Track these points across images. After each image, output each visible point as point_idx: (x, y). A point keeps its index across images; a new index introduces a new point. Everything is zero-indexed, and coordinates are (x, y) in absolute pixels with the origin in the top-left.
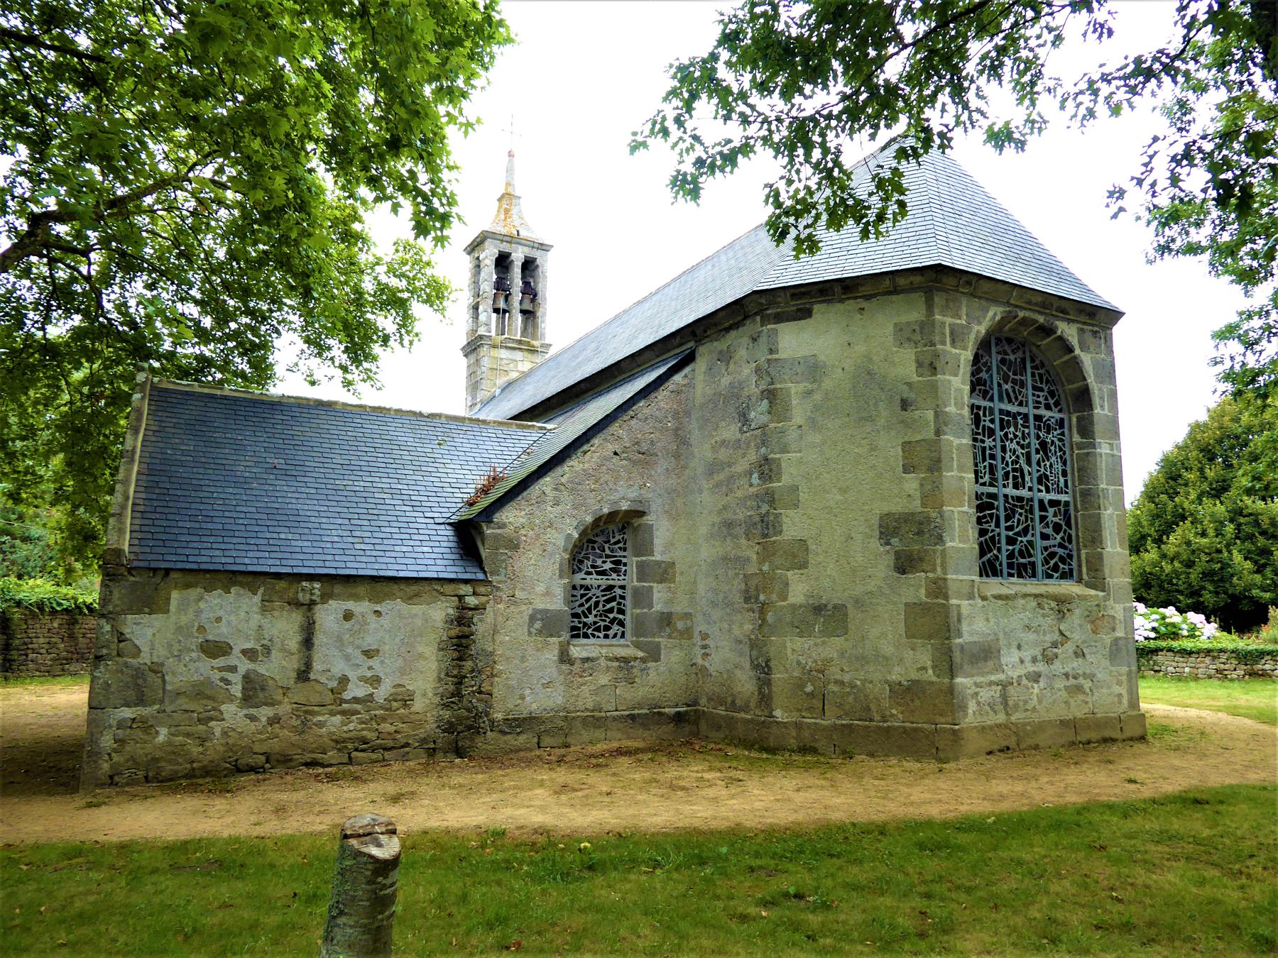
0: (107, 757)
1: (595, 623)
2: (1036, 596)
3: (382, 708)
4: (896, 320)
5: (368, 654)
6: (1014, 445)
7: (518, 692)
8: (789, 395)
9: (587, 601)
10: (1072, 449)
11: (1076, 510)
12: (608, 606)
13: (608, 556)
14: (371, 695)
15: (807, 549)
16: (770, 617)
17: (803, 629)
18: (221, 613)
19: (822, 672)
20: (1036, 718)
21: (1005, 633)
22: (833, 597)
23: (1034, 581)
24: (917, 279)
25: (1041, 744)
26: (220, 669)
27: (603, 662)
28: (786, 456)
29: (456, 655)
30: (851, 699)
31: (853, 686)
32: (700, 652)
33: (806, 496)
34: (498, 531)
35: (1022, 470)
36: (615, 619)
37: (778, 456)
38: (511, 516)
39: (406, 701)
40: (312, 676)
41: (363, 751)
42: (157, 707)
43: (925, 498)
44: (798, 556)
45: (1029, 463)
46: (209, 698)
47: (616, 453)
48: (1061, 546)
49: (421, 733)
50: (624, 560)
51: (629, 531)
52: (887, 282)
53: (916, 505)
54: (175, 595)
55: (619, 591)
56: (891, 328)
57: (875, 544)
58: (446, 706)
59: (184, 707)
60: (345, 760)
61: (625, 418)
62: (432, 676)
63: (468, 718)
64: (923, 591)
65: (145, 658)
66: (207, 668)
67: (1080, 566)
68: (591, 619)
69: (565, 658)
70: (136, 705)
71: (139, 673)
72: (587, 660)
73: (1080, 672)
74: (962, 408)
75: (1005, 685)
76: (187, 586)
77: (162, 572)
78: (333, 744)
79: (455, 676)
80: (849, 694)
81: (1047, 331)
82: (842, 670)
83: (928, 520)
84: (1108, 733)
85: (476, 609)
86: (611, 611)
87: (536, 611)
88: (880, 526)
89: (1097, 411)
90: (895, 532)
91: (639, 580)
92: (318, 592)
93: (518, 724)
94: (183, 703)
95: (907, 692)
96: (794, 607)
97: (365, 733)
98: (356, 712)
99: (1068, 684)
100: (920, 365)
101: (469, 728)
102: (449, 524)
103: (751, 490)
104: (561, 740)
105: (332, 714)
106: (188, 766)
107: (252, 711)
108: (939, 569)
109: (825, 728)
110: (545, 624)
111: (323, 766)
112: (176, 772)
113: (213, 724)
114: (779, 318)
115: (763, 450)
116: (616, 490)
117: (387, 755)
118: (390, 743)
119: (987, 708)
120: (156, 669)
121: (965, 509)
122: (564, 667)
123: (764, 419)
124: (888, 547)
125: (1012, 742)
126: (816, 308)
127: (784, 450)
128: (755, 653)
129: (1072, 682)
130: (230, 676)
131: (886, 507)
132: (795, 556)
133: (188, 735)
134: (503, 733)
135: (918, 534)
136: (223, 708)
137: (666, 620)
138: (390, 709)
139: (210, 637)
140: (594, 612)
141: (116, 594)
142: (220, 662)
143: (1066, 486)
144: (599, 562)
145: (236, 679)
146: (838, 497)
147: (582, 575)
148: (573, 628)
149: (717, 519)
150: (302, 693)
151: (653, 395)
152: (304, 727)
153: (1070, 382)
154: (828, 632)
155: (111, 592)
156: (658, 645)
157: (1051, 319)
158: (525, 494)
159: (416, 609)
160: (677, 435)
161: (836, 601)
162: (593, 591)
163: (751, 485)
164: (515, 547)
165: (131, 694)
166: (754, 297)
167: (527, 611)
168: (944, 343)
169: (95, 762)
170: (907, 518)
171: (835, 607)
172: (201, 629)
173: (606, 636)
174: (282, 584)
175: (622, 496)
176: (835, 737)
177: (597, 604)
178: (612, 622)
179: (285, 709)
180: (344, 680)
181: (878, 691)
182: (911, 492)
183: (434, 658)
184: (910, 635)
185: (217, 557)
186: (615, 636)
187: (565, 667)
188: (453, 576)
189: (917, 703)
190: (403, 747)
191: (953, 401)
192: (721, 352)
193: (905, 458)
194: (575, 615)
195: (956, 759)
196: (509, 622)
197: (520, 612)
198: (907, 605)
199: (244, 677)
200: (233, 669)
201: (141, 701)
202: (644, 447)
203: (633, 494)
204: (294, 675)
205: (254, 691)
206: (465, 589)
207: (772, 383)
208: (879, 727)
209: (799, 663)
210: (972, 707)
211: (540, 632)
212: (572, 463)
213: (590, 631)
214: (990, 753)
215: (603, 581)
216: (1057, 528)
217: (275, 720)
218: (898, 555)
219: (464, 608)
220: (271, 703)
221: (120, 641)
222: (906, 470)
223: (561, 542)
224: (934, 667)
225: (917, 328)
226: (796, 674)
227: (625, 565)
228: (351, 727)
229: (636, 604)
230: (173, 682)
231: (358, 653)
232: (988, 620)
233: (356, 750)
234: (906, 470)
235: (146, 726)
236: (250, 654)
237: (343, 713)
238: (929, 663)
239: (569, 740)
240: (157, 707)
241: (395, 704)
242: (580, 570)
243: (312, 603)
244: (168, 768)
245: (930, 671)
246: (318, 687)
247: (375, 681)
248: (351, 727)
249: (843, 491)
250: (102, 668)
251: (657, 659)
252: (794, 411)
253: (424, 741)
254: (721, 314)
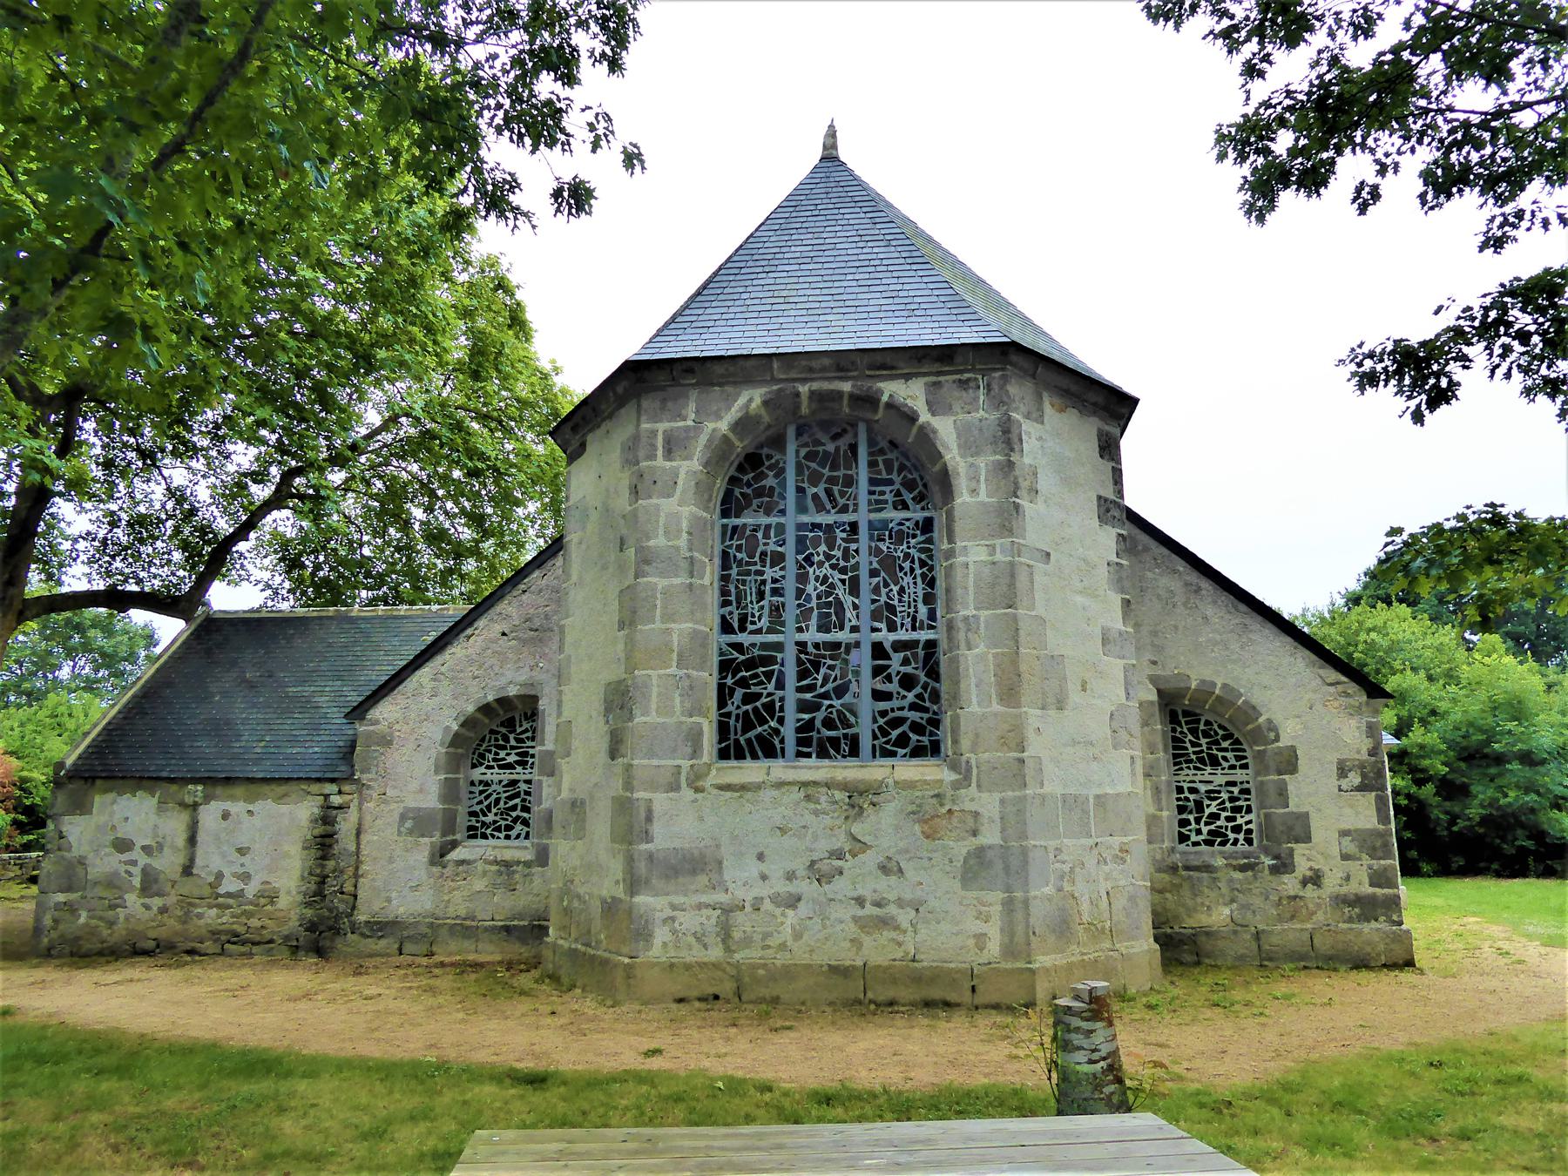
1: (495, 822)
2: (805, 784)
3: (251, 903)
5: (242, 851)
6: (826, 570)
7: (384, 894)
9: (487, 798)
12: (511, 803)
13: (513, 748)
18: (128, 814)
20: (782, 959)
21: (734, 838)
23: (852, 762)
25: (785, 997)
26: (126, 863)
27: (480, 866)
29: (320, 853)
34: (371, 728)
35: (839, 604)
36: (518, 817)
38: (385, 712)
40: (195, 871)
41: (234, 943)
45: (854, 589)
47: (504, 634)
48: (913, 707)
49: (285, 930)
50: (531, 751)
54: (97, 799)
55: (524, 787)
58: (308, 905)
61: (515, 593)
62: (296, 873)
63: (329, 918)
65: (75, 852)
68: (490, 818)
72: (463, 862)
73: (892, 896)
74: (678, 537)
75: (727, 910)
76: (106, 791)
79: (317, 876)
81: (868, 401)
84: (936, 993)
85: (340, 808)
86: (514, 808)
87: (407, 810)
92: (199, 794)
93: (380, 928)
97: (235, 927)
99: (860, 913)
101: (330, 929)
104: (424, 948)
105: (210, 907)
107: (147, 901)
113: (119, 910)
116: (502, 674)
117: (255, 949)
118: (257, 938)
119: (692, 940)
120: (81, 861)
122: (434, 869)
125: (727, 988)
129: (870, 910)
133: (101, 918)
134: (363, 935)
139: (119, 835)
140: (494, 810)
141: (59, 799)
142: (126, 856)
143: (932, 615)
144: (502, 754)
145: (136, 871)
147: (482, 769)
148: (470, 828)
150: (187, 887)
151: (550, 563)
152: (185, 919)
157: (867, 384)
159: (284, 809)
162: (494, 787)
164: (389, 743)
167: (397, 809)
168: (652, 457)
173: (508, 837)
175: (509, 681)
177: (497, 801)
178: (515, 820)
179: (171, 900)
185: (152, 768)
186: (518, 836)
187: (436, 870)
188: (318, 775)
191: (661, 532)
194: (473, 814)
196: (378, 822)
197: (392, 811)
201: (69, 889)
202: (537, 623)
203: (523, 677)
205: (150, 884)
206: (331, 788)
210: (661, 935)
212: (453, 650)
213: (489, 831)
214: (681, 1001)
215: (506, 776)
216: (907, 682)
217: (163, 910)
219: (329, 807)
220: (160, 894)
223: (438, 737)
227: (533, 756)
228: (224, 919)
232: (701, 819)
233: (229, 942)
236: (147, 849)
237: (219, 906)
239: (434, 949)
241: (262, 901)
242: (481, 764)
243: (195, 806)
247: (245, 877)
253: (287, 938)
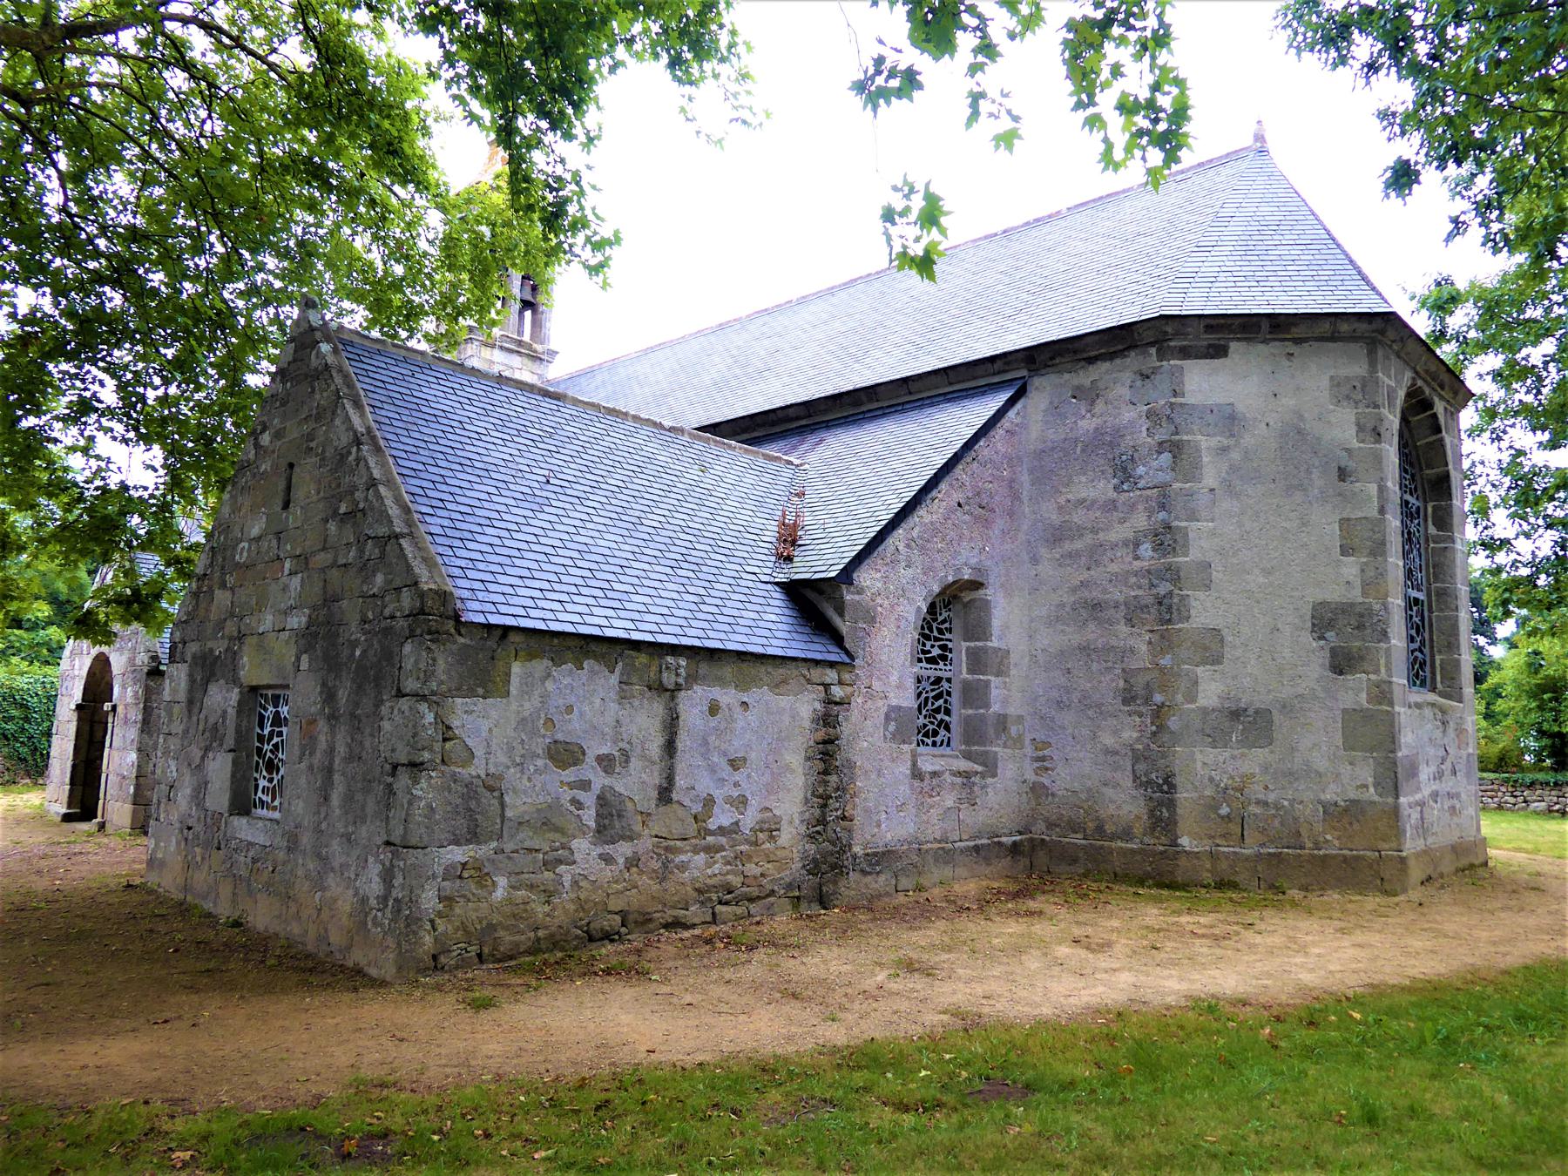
0: (428, 926)
4: (1332, 372)
8: (1198, 450)
10: (1427, 540)
11: (1430, 611)
12: (937, 704)
13: (936, 639)
14: (737, 823)
15: (1222, 641)
16: (1173, 723)
17: (1217, 738)
18: (572, 700)
19: (1241, 790)
22: (1260, 700)
24: (1363, 327)
26: (572, 786)
27: (948, 777)
28: (1194, 525)
30: (1277, 823)
31: (1278, 806)
33: (1220, 576)
36: (942, 721)
37: (1183, 524)
40: (675, 796)
41: (727, 903)
42: (494, 844)
43: (1366, 586)
44: (1212, 649)
46: (557, 829)
47: (959, 505)
49: (787, 876)
51: (957, 607)
52: (1327, 325)
53: (1356, 595)
54: (516, 668)
56: (1325, 382)
57: (1307, 639)
59: (527, 844)
60: (709, 918)
64: (1364, 695)
65: (477, 769)
66: (553, 784)
67: (1433, 673)
69: (917, 774)
70: (469, 842)
71: (470, 790)
76: (532, 656)
77: (499, 632)
78: (695, 894)
80: (1274, 816)
82: (1266, 788)
83: (1370, 612)
88: (1313, 617)
89: (1454, 502)
90: (1330, 625)
91: (970, 671)
94: (527, 838)
95: (1346, 814)
96: (1205, 712)
98: (722, 848)
100: (1360, 428)
101: (834, 867)
102: (777, 584)
103: (1137, 563)
105: (696, 851)
106: (532, 935)
107: (608, 848)
108: (1383, 670)
109: (1247, 859)
111: (686, 927)
112: (517, 944)
113: (562, 868)
114: (1185, 353)
115: (1162, 515)
117: (754, 908)
118: (754, 891)
120: (493, 785)
123: (1163, 477)
124: (1322, 643)
126: (1233, 346)
127: (1193, 517)
128: (1142, 767)
130: (581, 795)
131: (1320, 596)
132: (1206, 649)
135: (1358, 628)
136: (575, 844)
138: (756, 844)
139: (560, 737)
141: (441, 664)
142: (570, 775)
145: (588, 799)
146: (1261, 580)
149: (1069, 599)
151: (992, 433)
153: (1429, 466)
154: (1248, 742)
155: (434, 660)
158: (880, 549)
160: (1011, 487)
161: (1258, 705)
163: (1137, 558)
165: (461, 823)
166: (1157, 323)
169: (415, 933)
170: (1345, 609)
171: (1257, 712)
172: (550, 721)
173: (934, 744)
174: (642, 659)
175: (963, 561)
176: (1259, 868)
180: (709, 802)
181: (1308, 811)
182: (1351, 578)
183: (800, 770)
184: (1349, 746)
189: (1356, 826)
190: (768, 896)
192: (1078, 388)
193: (1342, 537)
195: (1405, 891)
198: (1345, 711)
199: (599, 797)
200: (585, 785)
204: (655, 794)
206: (831, 675)
207: (1177, 434)
208: (1314, 856)
209: (1211, 779)
217: (633, 862)
218: (1334, 652)
221: (445, 740)
222: (1346, 550)
224: (1376, 785)
225: (1359, 386)
226: (1207, 793)
228: (717, 868)
229: (966, 702)
230: (517, 806)
231: (723, 763)
233: (720, 903)
234: (1346, 550)
235: (479, 873)
237: (708, 849)
238: (1371, 780)
240: (494, 844)
241: (761, 835)
244: (507, 938)
245: (1372, 790)
246: (680, 812)
248: (717, 868)
249: (1267, 572)
250: (424, 784)
251: (994, 775)
252: (1205, 470)
254: (1089, 339)
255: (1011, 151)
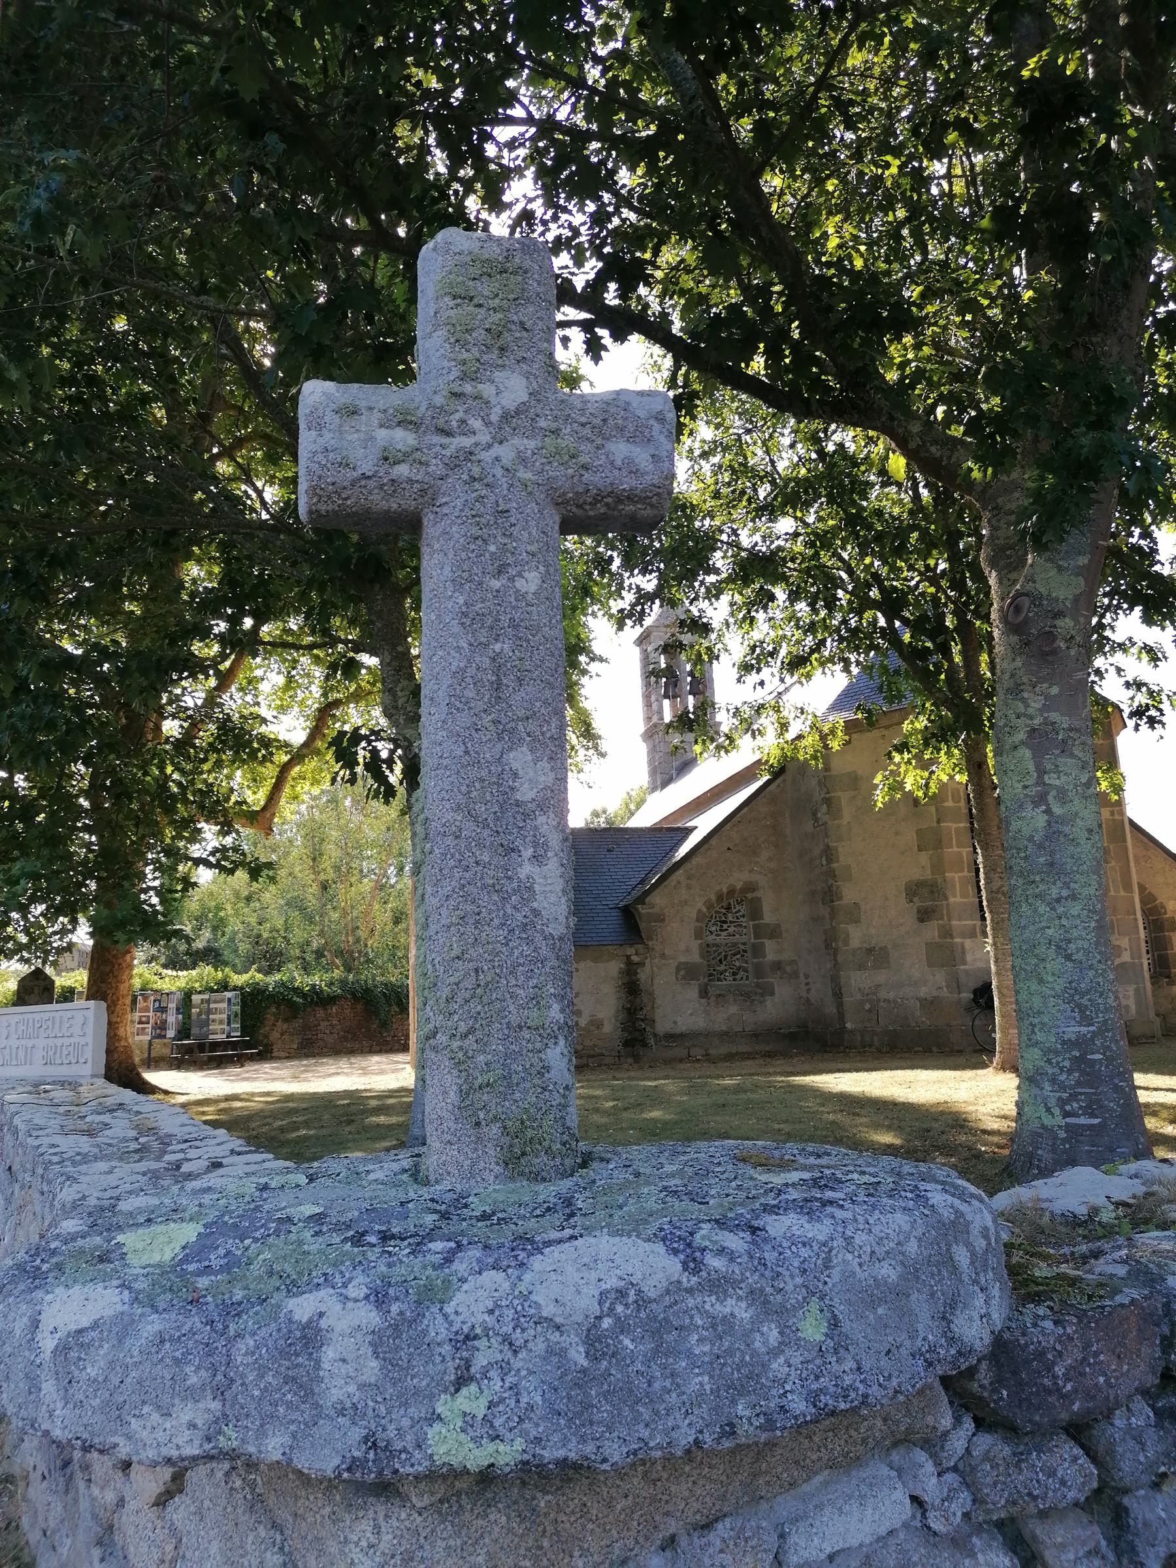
17: (861, 967)
31: (895, 1001)
32: (805, 988)
39: (598, 1024)
53: (928, 875)
93: (673, 1037)
110: (688, 972)
121: (965, 873)
137: (778, 966)
156: (772, 984)
170: (921, 884)
211: (684, 978)
222: (920, 850)
234: (920, 850)
255: (603, 755)
